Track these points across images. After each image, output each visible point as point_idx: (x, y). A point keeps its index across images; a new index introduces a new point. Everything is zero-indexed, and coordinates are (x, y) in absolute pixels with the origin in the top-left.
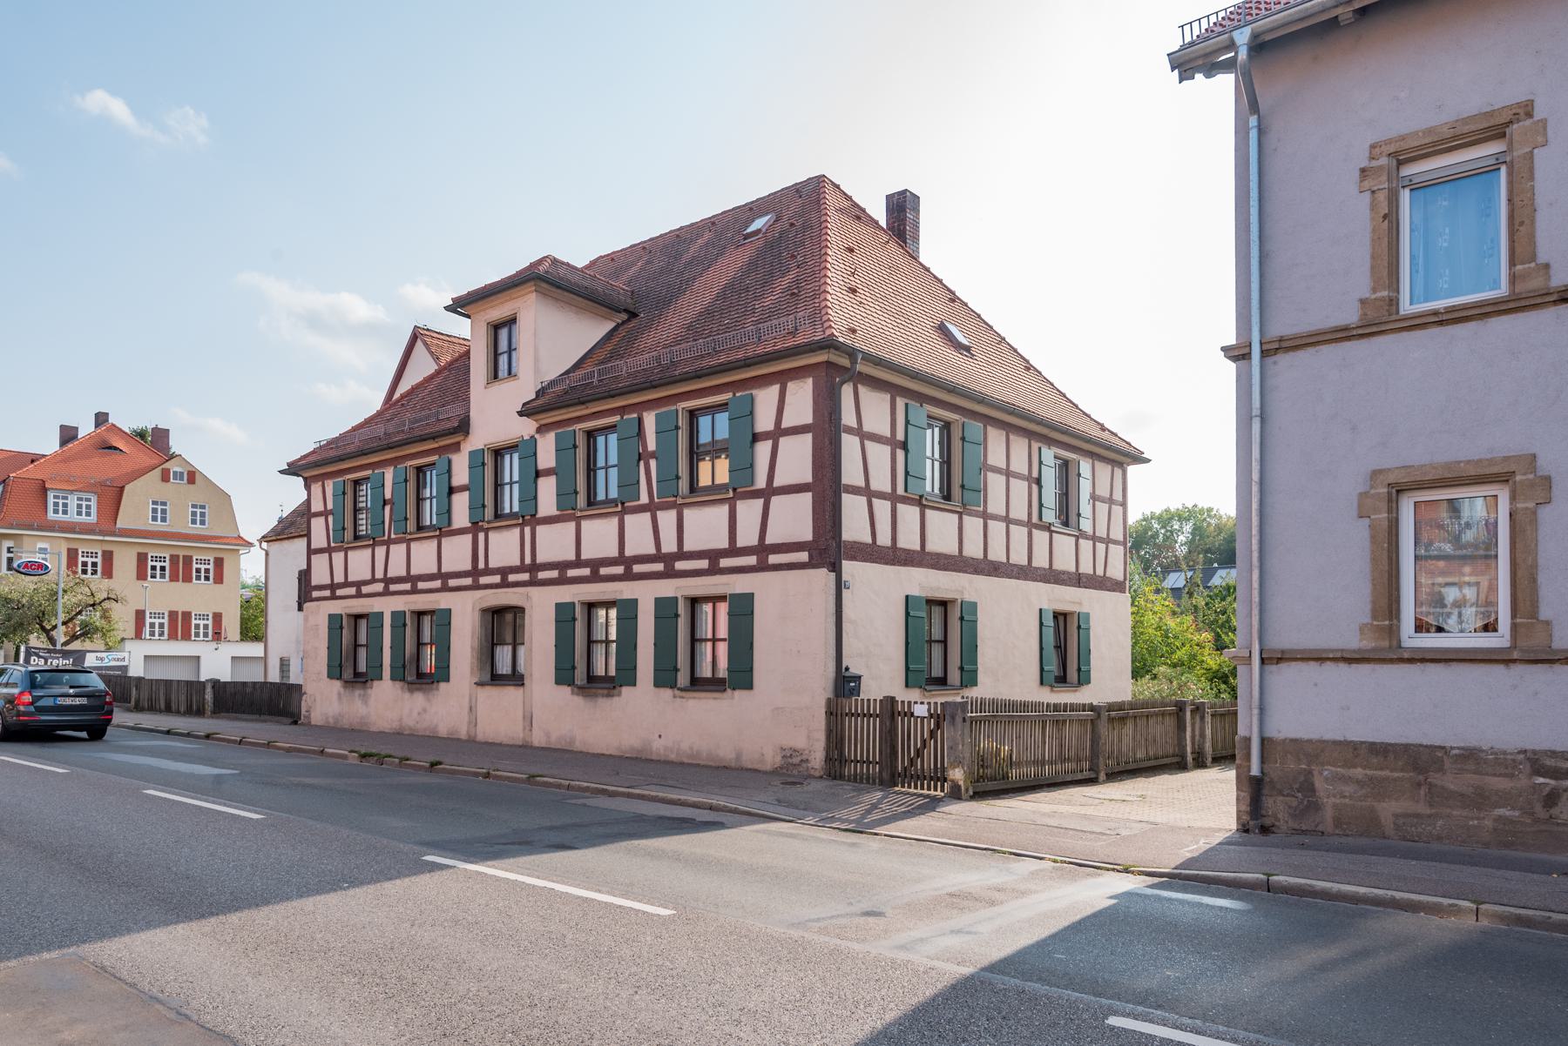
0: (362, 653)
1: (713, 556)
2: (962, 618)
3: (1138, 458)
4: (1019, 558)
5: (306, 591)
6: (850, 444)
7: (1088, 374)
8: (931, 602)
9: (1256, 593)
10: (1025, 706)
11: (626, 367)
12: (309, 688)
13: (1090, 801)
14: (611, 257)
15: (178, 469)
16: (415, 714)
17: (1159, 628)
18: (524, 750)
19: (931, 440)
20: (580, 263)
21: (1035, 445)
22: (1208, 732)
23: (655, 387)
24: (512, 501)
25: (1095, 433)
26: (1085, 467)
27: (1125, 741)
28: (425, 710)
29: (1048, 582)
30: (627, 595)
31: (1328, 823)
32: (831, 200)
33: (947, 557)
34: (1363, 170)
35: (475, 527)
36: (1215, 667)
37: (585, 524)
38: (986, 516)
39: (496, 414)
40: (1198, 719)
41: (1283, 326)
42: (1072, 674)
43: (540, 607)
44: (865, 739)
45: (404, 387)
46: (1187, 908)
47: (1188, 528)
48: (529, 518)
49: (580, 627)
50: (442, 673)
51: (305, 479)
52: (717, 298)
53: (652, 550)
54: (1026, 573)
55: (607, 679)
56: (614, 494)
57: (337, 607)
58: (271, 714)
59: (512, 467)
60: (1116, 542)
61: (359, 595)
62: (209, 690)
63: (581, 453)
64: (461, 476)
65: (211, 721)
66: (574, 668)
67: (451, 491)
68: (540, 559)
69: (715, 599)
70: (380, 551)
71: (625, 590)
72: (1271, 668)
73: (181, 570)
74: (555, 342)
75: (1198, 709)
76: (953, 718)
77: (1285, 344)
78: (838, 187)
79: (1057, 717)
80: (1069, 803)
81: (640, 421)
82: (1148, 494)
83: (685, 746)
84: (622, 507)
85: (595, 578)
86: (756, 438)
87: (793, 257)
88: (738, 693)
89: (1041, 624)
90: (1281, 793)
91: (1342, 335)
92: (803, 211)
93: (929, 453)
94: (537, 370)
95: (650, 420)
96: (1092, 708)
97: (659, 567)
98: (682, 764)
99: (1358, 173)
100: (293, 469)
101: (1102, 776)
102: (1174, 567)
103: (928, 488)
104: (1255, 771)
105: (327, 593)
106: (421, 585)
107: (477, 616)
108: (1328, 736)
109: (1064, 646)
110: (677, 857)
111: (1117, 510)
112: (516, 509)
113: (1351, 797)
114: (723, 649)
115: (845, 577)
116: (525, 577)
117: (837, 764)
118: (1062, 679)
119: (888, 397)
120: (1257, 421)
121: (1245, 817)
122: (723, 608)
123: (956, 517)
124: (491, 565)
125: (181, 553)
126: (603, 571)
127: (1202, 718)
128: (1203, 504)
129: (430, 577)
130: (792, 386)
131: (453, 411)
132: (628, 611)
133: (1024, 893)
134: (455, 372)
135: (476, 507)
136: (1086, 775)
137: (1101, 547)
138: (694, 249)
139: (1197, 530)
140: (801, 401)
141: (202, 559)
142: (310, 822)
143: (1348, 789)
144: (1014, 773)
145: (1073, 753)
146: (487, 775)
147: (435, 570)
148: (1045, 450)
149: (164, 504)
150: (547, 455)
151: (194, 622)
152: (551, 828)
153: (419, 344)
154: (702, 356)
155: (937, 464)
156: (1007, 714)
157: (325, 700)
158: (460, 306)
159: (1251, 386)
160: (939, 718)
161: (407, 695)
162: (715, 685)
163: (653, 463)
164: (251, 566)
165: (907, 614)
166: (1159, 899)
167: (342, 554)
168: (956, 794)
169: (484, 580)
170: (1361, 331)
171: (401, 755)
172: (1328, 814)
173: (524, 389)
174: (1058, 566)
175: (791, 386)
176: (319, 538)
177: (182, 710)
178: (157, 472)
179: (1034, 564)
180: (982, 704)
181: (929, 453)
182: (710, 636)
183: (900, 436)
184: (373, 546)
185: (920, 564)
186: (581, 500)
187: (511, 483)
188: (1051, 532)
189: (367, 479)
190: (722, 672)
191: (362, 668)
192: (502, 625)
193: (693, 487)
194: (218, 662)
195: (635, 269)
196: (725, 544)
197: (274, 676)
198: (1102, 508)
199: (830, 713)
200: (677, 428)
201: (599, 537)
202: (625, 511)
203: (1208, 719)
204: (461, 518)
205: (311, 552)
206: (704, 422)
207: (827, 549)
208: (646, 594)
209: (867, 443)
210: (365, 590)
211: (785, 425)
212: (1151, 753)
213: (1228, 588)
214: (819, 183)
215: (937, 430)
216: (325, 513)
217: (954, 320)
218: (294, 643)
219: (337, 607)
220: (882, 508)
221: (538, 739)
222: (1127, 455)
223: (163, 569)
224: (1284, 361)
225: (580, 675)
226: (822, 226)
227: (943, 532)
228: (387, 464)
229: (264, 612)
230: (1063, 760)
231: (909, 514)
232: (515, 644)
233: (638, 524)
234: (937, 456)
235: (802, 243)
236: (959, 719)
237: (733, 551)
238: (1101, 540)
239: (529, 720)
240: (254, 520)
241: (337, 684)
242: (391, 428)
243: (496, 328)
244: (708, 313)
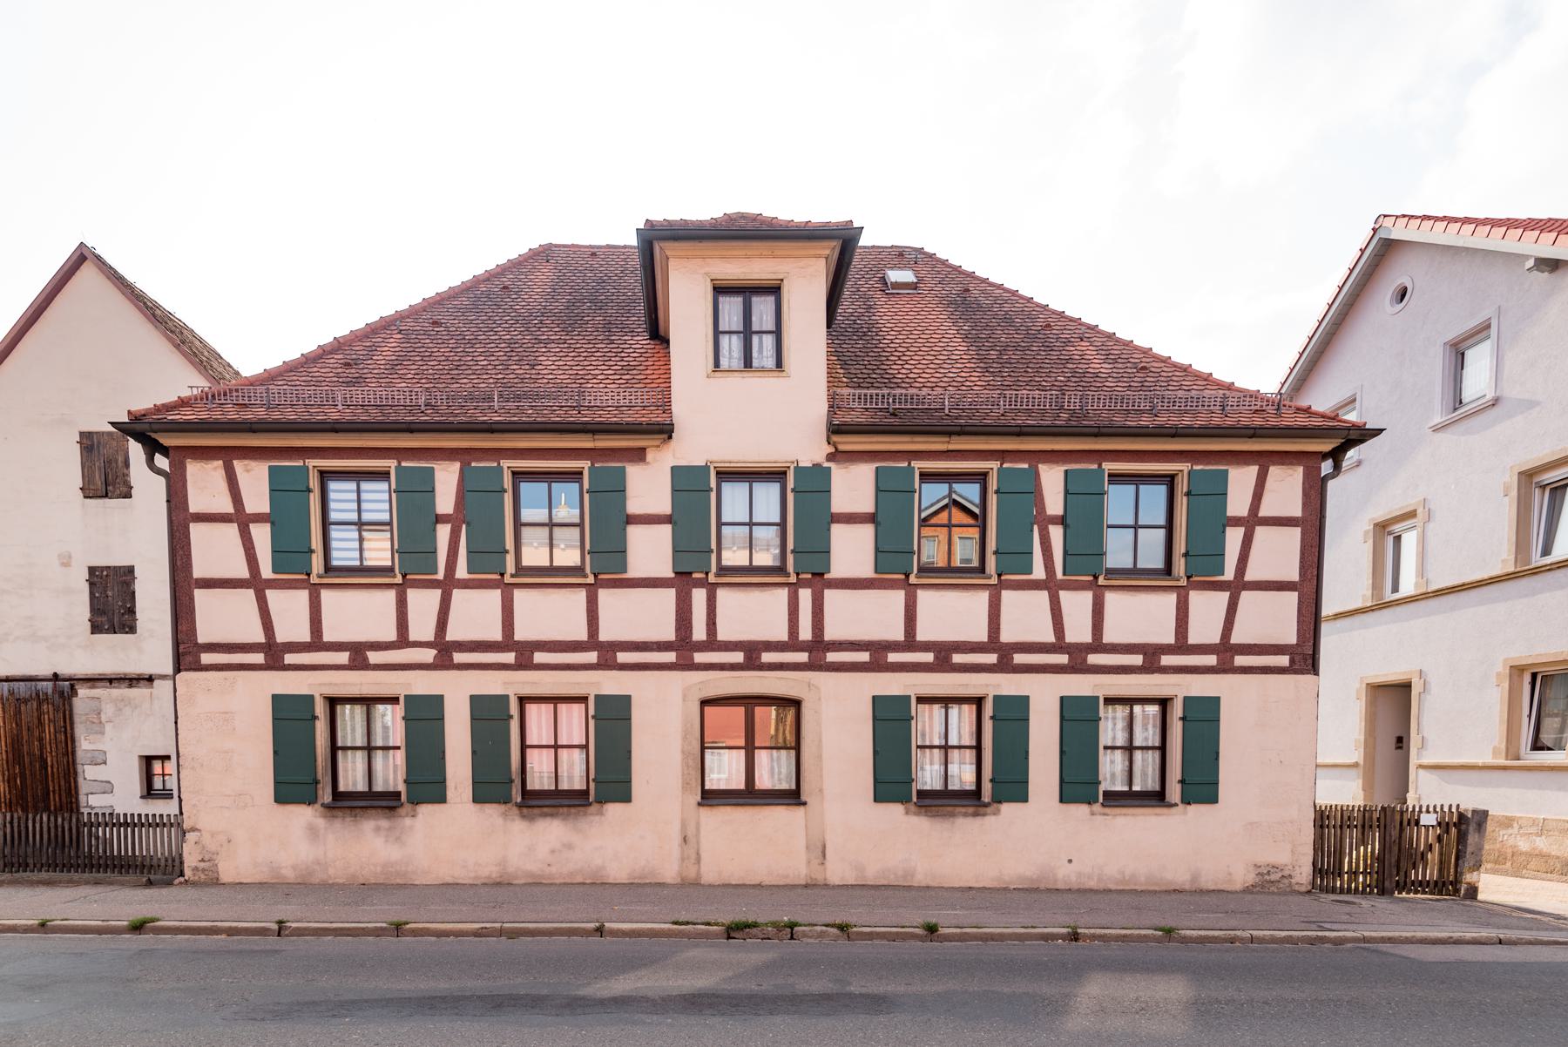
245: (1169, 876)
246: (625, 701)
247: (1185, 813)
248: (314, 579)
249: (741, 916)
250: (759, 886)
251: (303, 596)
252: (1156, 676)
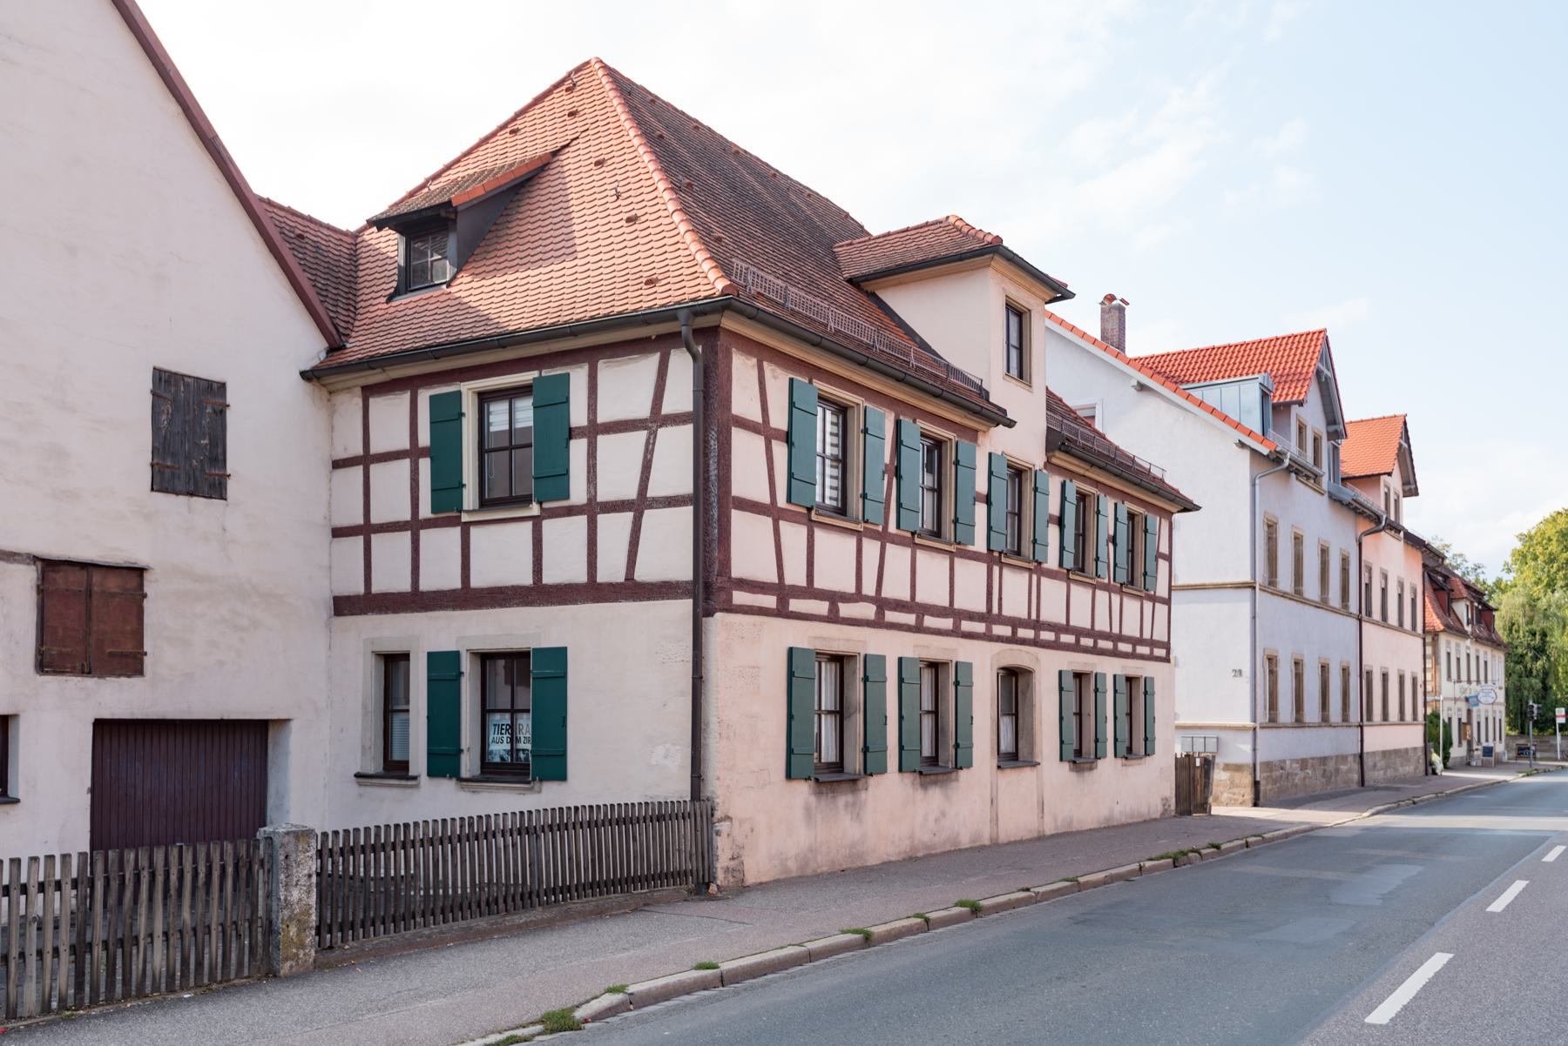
3: (1188, 507)
16: (932, 818)
28: (943, 814)
42: (1139, 745)
61: (833, 618)
93: (819, 449)
123: (852, 542)
161: (920, 793)
181: (819, 449)
209: (758, 418)
248: (465, 518)
251: (455, 533)
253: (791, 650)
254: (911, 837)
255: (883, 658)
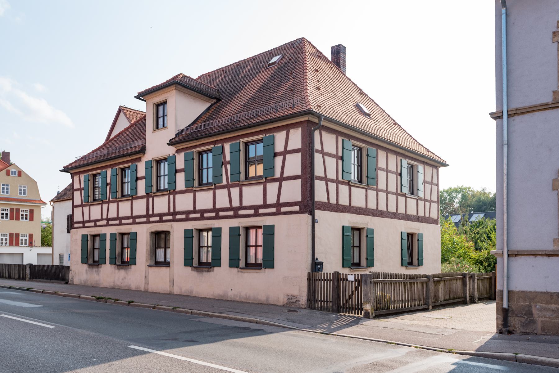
0: (97, 252)
1: (256, 208)
2: (367, 236)
3: (444, 164)
4: (392, 209)
5: (71, 224)
6: (318, 157)
7: (421, 128)
8: (353, 229)
9: (505, 225)
10: (397, 276)
11: (217, 123)
12: (72, 268)
13: (427, 319)
14: (208, 75)
15: (14, 170)
17: (450, 241)
18: (170, 295)
19: (353, 156)
20: (195, 76)
21: (399, 158)
22: (476, 287)
23: (230, 132)
24: (164, 183)
25: (425, 153)
26: (421, 168)
27: (439, 291)
28: (125, 278)
29: (405, 220)
30: (216, 226)
31: (539, 329)
32: (307, 48)
33: (360, 208)
34: (554, 33)
35: (148, 195)
36: (477, 258)
37: (198, 194)
38: (377, 190)
39: (157, 144)
40: (471, 281)
41: (517, 104)
42: (415, 261)
43: (177, 232)
44: (325, 291)
45: (115, 133)
46: (481, 370)
47: (460, 196)
48: (172, 191)
49: (195, 240)
50: (133, 261)
51: (71, 174)
52: (257, 92)
53: (228, 206)
54: (395, 216)
55: (207, 264)
56: (210, 180)
57: (85, 231)
58: (56, 279)
59: (165, 168)
60: (434, 202)
61: (96, 226)
62: (28, 269)
63: (196, 162)
64: (141, 172)
65: (29, 283)
66: (192, 259)
67: (137, 179)
68: (177, 210)
69: (257, 228)
70: (105, 206)
71: (216, 224)
72: (511, 259)
73: (15, 215)
74: (185, 112)
75: (472, 277)
76: (366, 281)
77: (518, 112)
78: (310, 43)
79: (411, 281)
80: (418, 320)
81: (223, 147)
82: (448, 180)
83: (243, 294)
84: (214, 186)
85: (202, 218)
86: (275, 155)
87: (291, 74)
88: (267, 270)
89: (402, 239)
90: (517, 316)
91: (545, 107)
92: (293, 56)
93: (352, 162)
94: (176, 125)
95: (227, 147)
96: (426, 276)
97: (231, 213)
98: (242, 302)
99: (551, 34)
100: (66, 170)
101: (431, 307)
102: (454, 212)
103: (352, 178)
104: (505, 306)
105: (81, 225)
106: (123, 222)
107: (149, 235)
108: (539, 290)
109: (411, 249)
110: (245, 346)
111: (435, 187)
112: (166, 187)
113: (549, 318)
114: (260, 250)
115: (316, 218)
116: (170, 218)
117: (312, 302)
118: (411, 264)
119: (335, 136)
120: (505, 147)
121: (501, 327)
122: (260, 232)
123: (364, 190)
124: (155, 213)
125: (15, 207)
126: (206, 215)
127: (474, 281)
128: (466, 185)
129: (128, 218)
130: (292, 131)
131: (138, 145)
132: (217, 233)
133: (405, 363)
134: (139, 126)
135: (148, 186)
136: (424, 307)
137: (428, 204)
138: (245, 71)
139: (464, 197)
140: (296, 138)
141: (24, 210)
142: (77, 330)
143: (548, 314)
144: (392, 306)
145: (418, 297)
146: (154, 307)
147: (130, 215)
148: (403, 160)
149: (7, 185)
150: (180, 163)
151: (20, 238)
152: (186, 332)
153: (122, 114)
154: (251, 118)
155: (356, 167)
156: (388, 279)
157: (80, 273)
158: (141, 96)
159: (503, 131)
160: (359, 281)
161: (117, 271)
162: (256, 266)
163: (229, 166)
164: (46, 213)
165: (343, 234)
166: (468, 365)
167: (88, 208)
168: (367, 316)
169: (152, 219)
170: (553, 106)
171: (115, 298)
172: (539, 325)
173: (170, 133)
174: (409, 212)
175: (292, 131)
176: (78, 201)
177: (16, 277)
178: (5, 171)
179: (399, 212)
180: (378, 275)
182: (254, 244)
183: (340, 154)
184: (102, 204)
185: (349, 212)
186: (196, 183)
187: (164, 176)
188: (406, 197)
189: (99, 174)
190: (260, 261)
191: (97, 259)
192: (160, 239)
193: (247, 178)
194: (31, 256)
195: (219, 79)
196: (192, 209)
197: (56, 263)
198: (428, 186)
199: (309, 279)
200: (240, 150)
201: (204, 200)
202: (216, 188)
203: (476, 281)
204: (181, 184)
205: (74, 207)
206: (252, 148)
207: (308, 205)
208: (225, 225)
209: (325, 157)
210: (98, 223)
211: (288, 149)
212: (451, 297)
213: (479, 222)
214: (303, 39)
215: (356, 151)
216: (80, 189)
217: (362, 102)
218: (66, 248)
219: (85, 231)
220: (332, 186)
221: (176, 291)
222: (439, 163)
223: (7, 214)
224: (518, 119)
225: (195, 262)
226: (304, 60)
227: (359, 197)
228: (109, 166)
229: (52, 233)
230: (414, 300)
231: (344, 189)
232: (166, 248)
233: (222, 194)
234: (356, 163)
235: (295, 68)
236: (369, 282)
237: (265, 206)
238: (428, 201)
239: (172, 282)
240: (47, 193)
241: (85, 266)
242: (110, 151)
243: (158, 106)
244: (253, 99)
245: (259, 297)
246: (273, 227)
247: (265, 272)
249: (101, 296)
250: (159, 293)
252: (258, 217)
253: (343, 226)
254: (114, 282)
255: (106, 234)
